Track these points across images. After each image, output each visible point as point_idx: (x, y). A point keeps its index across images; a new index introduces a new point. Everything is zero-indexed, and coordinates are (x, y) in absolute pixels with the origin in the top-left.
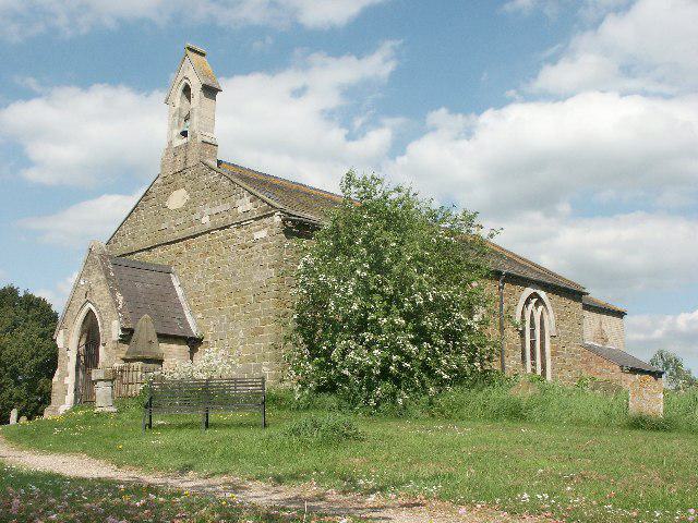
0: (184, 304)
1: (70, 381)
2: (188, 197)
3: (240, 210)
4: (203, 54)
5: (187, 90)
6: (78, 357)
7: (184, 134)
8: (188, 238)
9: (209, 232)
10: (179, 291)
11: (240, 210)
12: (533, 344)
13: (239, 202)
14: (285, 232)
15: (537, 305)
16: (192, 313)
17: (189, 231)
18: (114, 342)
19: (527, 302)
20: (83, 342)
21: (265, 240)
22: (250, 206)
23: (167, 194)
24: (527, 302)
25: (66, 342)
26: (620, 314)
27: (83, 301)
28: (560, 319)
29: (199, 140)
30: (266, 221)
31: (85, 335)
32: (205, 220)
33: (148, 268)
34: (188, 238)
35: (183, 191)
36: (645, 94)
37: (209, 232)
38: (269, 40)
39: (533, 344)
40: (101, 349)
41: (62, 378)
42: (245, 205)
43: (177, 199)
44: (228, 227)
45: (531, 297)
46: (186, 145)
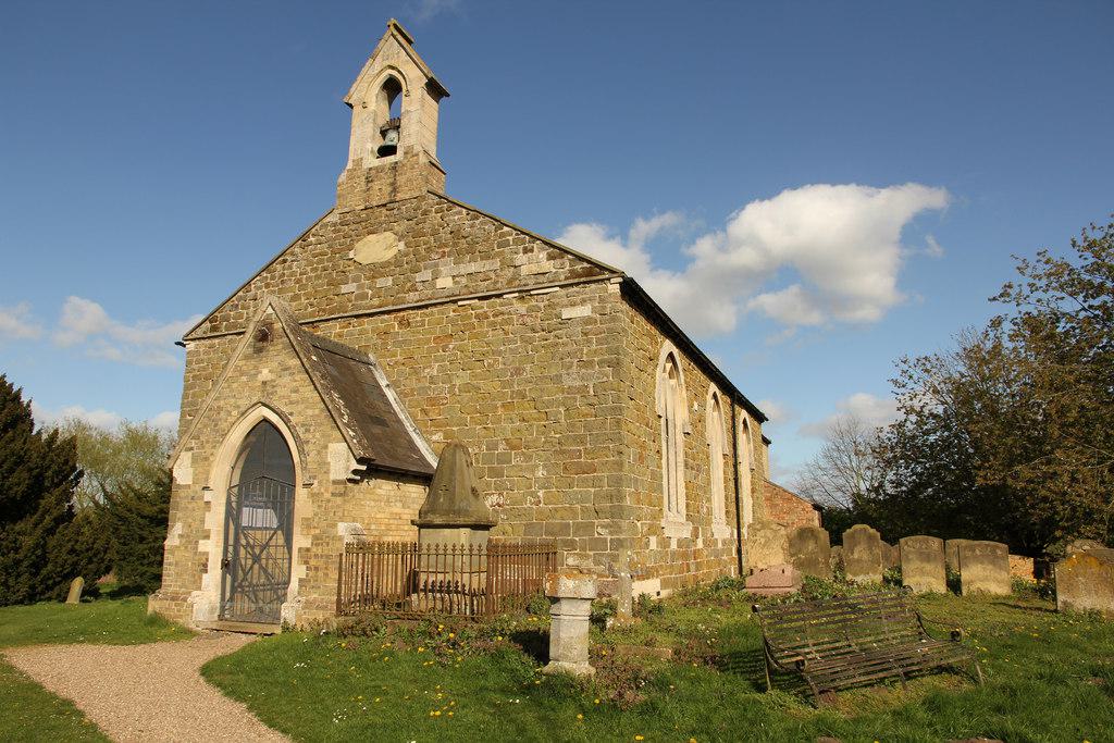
2: (402, 246)
7: (387, 151)
10: (390, 395)
11: (524, 270)
18: (335, 482)
20: (236, 481)
21: (587, 321)
27: (244, 403)
40: (301, 493)
43: (377, 248)
46: (394, 167)
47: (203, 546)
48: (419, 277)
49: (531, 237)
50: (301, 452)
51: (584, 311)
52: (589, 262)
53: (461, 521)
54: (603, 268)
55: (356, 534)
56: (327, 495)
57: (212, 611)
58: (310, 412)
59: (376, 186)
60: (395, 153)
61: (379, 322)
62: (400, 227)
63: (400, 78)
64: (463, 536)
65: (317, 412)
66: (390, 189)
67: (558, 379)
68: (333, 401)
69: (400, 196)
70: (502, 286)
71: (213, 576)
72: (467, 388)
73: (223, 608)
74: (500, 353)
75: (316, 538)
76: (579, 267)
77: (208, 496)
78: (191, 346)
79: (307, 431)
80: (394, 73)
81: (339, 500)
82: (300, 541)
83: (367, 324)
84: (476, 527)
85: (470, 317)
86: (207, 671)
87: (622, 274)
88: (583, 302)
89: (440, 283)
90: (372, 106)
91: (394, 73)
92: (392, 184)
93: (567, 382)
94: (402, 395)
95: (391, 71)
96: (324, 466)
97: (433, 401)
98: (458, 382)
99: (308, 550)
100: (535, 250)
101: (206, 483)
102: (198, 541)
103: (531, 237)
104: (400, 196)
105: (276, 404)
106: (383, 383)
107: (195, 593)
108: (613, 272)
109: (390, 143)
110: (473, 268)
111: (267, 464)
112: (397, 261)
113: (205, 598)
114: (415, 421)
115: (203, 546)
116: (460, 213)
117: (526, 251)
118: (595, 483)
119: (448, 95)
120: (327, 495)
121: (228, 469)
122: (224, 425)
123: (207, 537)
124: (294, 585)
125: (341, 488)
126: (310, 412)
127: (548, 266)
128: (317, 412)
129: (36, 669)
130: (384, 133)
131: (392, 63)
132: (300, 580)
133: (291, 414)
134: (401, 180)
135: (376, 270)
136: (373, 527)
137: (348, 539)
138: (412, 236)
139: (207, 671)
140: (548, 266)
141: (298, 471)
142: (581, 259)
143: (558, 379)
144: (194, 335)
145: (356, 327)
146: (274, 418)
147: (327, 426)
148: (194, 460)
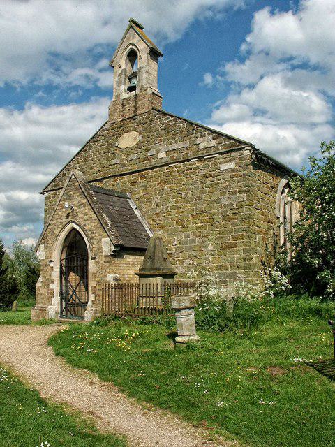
0: (143, 223)
1: (55, 287)
2: (140, 138)
3: (201, 146)
6: (61, 267)
7: (131, 89)
8: (143, 170)
9: (167, 165)
10: (137, 213)
11: (201, 146)
13: (199, 140)
14: (253, 164)
17: (143, 165)
18: (106, 256)
20: (64, 256)
21: (233, 170)
23: (118, 136)
25: (49, 255)
27: (65, 221)
29: (149, 92)
30: (234, 154)
31: (66, 249)
32: (162, 155)
33: (110, 193)
34: (143, 170)
35: (134, 134)
36: (262, 123)
37: (167, 165)
38: (80, 92)
40: (91, 262)
41: (46, 284)
43: (128, 140)
44: (189, 160)
46: (136, 97)
47: (51, 286)
48: (149, 153)
49: (204, 128)
50: (91, 243)
51: (232, 165)
52: (234, 139)
53: (157, 272)
54: (241, 142)
55: (116, 279)
56: (102, 262)
57: (57, 313)
58: (93, 224)
59: (127, 108)
60: (135, 90)
61: (131, 177)
62: (140, 128)
63: (136, 49)
64: (159, 280)
65: (96, 224)
66: (134, 109)
67: (218, 201)
68: (103, 218)
69: (139, 112)
70: (190, 156)
71: (56, 299)
72: (174, 208)
73: (62, 311)
74: (189, 190)
75: (98, 282)
76: (229, 142)
77: (52, 264)
78: (47, 194)
79: (92, 233)
80: (134, 47)
81: (107, 264)
82: (92, 283)
83: (126, 178)
84: (164, 276)
85: (174, 171)
86: (51, 342)
87: (252, 146)
88: (230, 161)
89: (160, 155)
90: (123, 66)
91: (134, 47)
92: (135, 106)
93: (224, 202)
94: (143, 213)
95: (131, 47)
96: (100, 248)
97: (158, 215)
98: (170, 205)
99: (95, 287)
100: (207, 135)
101: (52, 258)
102: (51, 284)
103: (204, 128)
104: (139, 112)
105: (78, 220)
106: (134, 207)
107: (49, 307)
108: (246, 144)
109: (133, 85)
110: (176, 146)
111: (76, 252)
112: (139, 146)
113: (54, 307)
114: (150, 225)
115: (51, 286)
116: (168, 118)
117: (202, 136)
118: (237, 252)
119: (162, 55)
120: (102, 262)
121: (60, 251)
122: (56, 232)
123: (53, 282)
124: (90, 303)
125: (108, 259)
126: (93, 224)
127: (213, 143)
128: (96, 224)
129: (22, 335)
130: (130, 79)
131: (131, 42)
132: (92, 301)
133: (85, 225)
134: (139, 103)
135: (131, 150)
136: (126, 276)
137: (113, 282)
138: (146, 134)
139: (51, 342)
140: (213, 143)
141: (89, 252)
142: (229, 138)
143: (218, 201)
144: (47, 189)
145: (120, 180)
146: (78, 228)
147: (101, 231)
148: (45, 248)
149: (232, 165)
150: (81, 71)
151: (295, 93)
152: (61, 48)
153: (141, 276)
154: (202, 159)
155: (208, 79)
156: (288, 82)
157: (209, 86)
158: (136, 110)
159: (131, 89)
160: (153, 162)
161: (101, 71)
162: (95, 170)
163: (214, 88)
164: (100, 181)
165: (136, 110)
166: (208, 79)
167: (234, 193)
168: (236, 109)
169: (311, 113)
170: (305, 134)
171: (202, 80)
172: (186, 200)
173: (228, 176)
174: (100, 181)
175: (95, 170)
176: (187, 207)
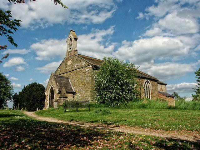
1: (48, 102)
4: (74, 32)
5: (71, 39)
6: (50, 97)
7: (70, 49)
10: (70, 82)
12: (147, 91)
13: (83, 63)
15: (148, 83)
16: (73, 87)
19: (146, 83)
21: (88, 71)
22: (85, 64)
24: (146, 83)
26: (165, 85)
28: (153, 86)
32: (76, 67)
36: (168, 36)
39: (147, 91)
40: (54, 95)
42: (84, 63)
43: (69, 63)
45: (146, 81)
51: (88, 69)
106: (70, 81)
118: (88, 92)
149: (88, 69)
150: (84, 16)
151: (183, 20)
152: (75, 7)
153: (60, 97)
154: (83, 68)
155: (141, 15)
156: (180, 14)
157: (142, 19)
158: (71, 55)
159: (70, 49)
160: (74, 69)
161: (92, 15)
162: (63, 71)
163: (144, 19)
164: (64, 74)
165: (71, 55)
166: (141, 15)
167: (88, 77)
168: (156, 30)
169: (190, 28)
170: (186, 39)
171: (138, 15)
172: (80, 79)
173: (87, 72)
174: (64, 74)
175: (63, 71)
176: (80, 80)
